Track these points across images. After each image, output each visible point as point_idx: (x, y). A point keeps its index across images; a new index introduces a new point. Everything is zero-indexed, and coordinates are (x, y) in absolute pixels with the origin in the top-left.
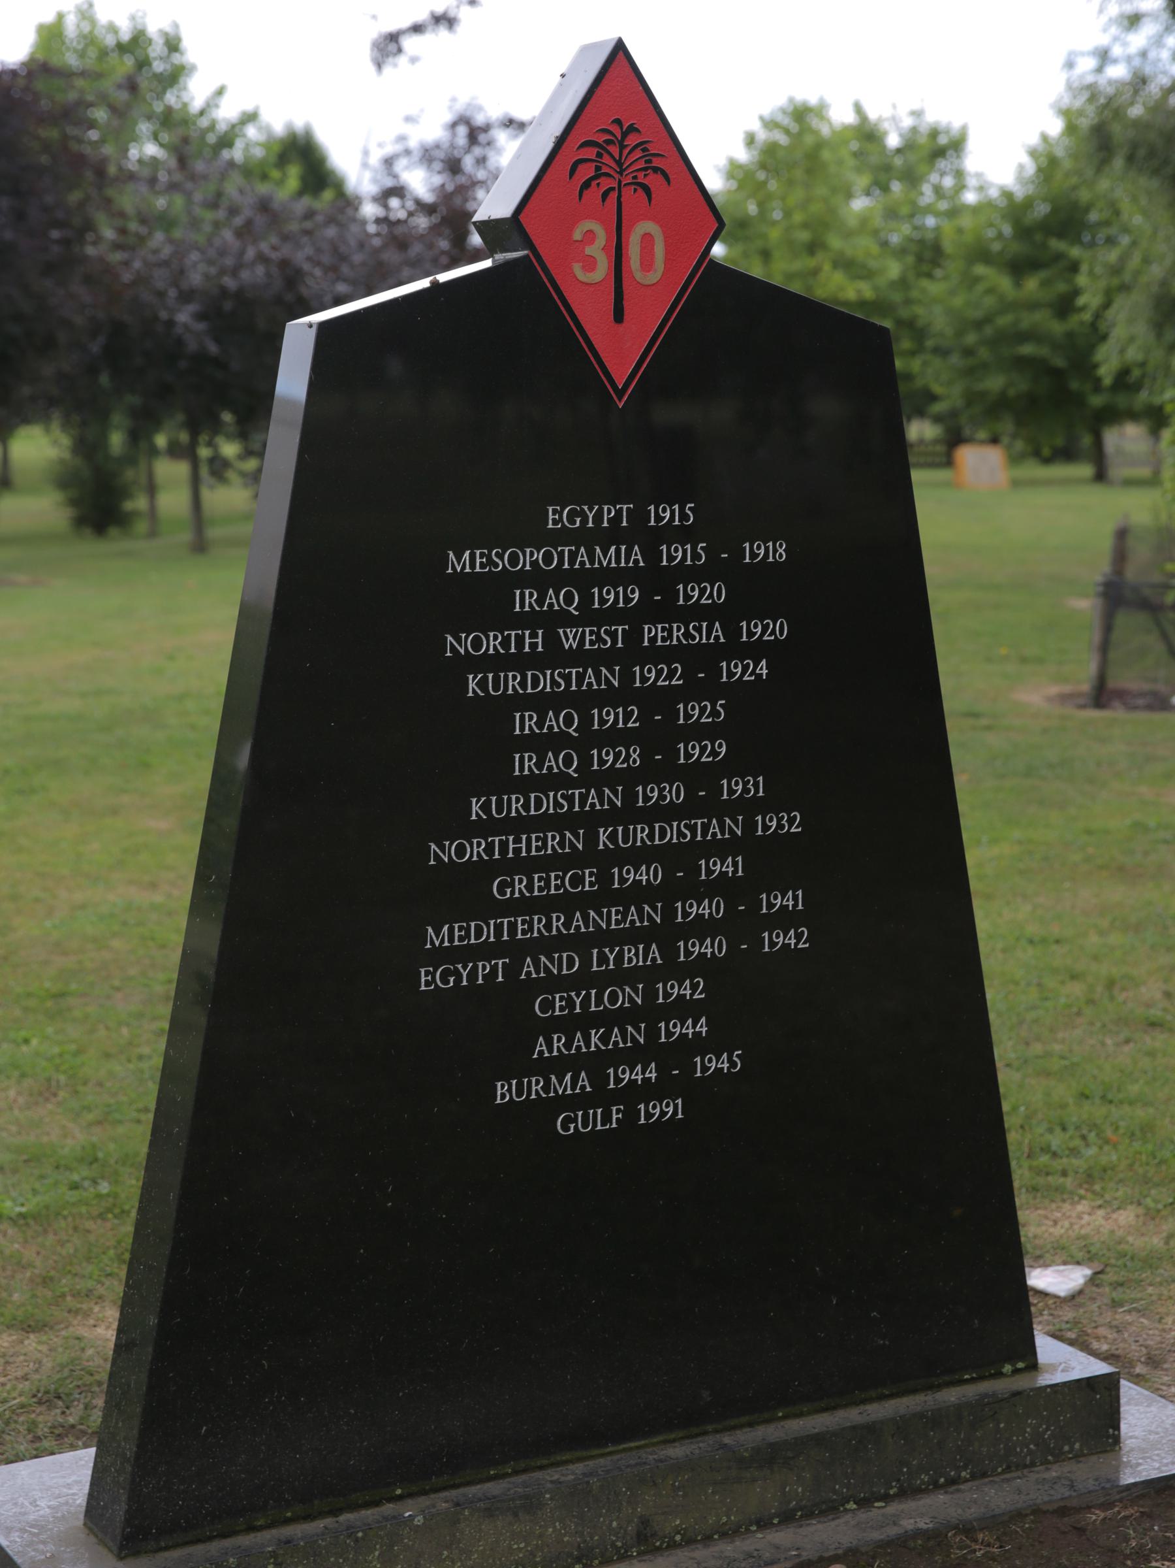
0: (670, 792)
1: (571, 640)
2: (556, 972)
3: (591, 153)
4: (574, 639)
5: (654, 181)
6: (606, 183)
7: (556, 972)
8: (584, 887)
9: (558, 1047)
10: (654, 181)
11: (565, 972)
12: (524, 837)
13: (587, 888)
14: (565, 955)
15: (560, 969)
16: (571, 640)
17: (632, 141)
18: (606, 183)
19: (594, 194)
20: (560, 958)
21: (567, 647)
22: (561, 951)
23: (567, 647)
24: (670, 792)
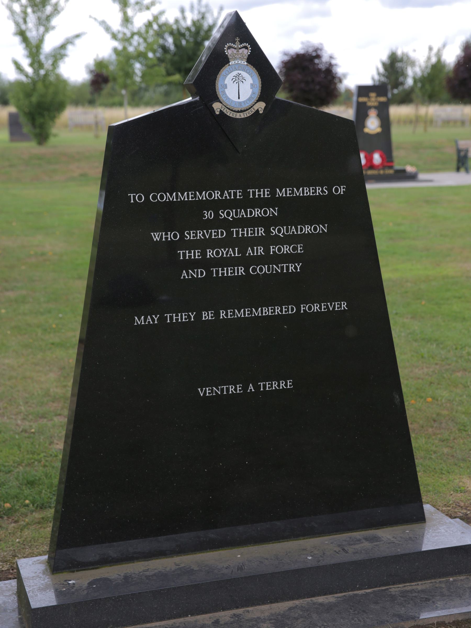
0: (207, 214)
1: (157, 237)
2: (196, 276)
3: (235, 77)
4: (158, 237)
5: (243, 81)
6: (237, 81)
7: (196, 276)
8: (298, 251)
9: (232, 391)
10: (243, 81)
11: (199, 276)
12: (246, 229)
13: (299, 252)
14: (199, 270)
15: (197, 275)
16: (157, 237)
17: (240, 75)
18: (237, 81)
19: (235, 82)
20: (197, 271)
21: (155, 240)
22: (197, 269)
23: (155, 240)
24: (207, 214)
